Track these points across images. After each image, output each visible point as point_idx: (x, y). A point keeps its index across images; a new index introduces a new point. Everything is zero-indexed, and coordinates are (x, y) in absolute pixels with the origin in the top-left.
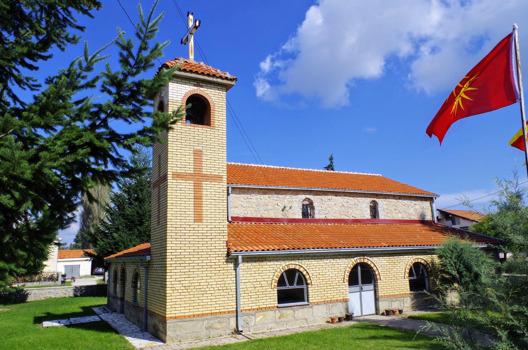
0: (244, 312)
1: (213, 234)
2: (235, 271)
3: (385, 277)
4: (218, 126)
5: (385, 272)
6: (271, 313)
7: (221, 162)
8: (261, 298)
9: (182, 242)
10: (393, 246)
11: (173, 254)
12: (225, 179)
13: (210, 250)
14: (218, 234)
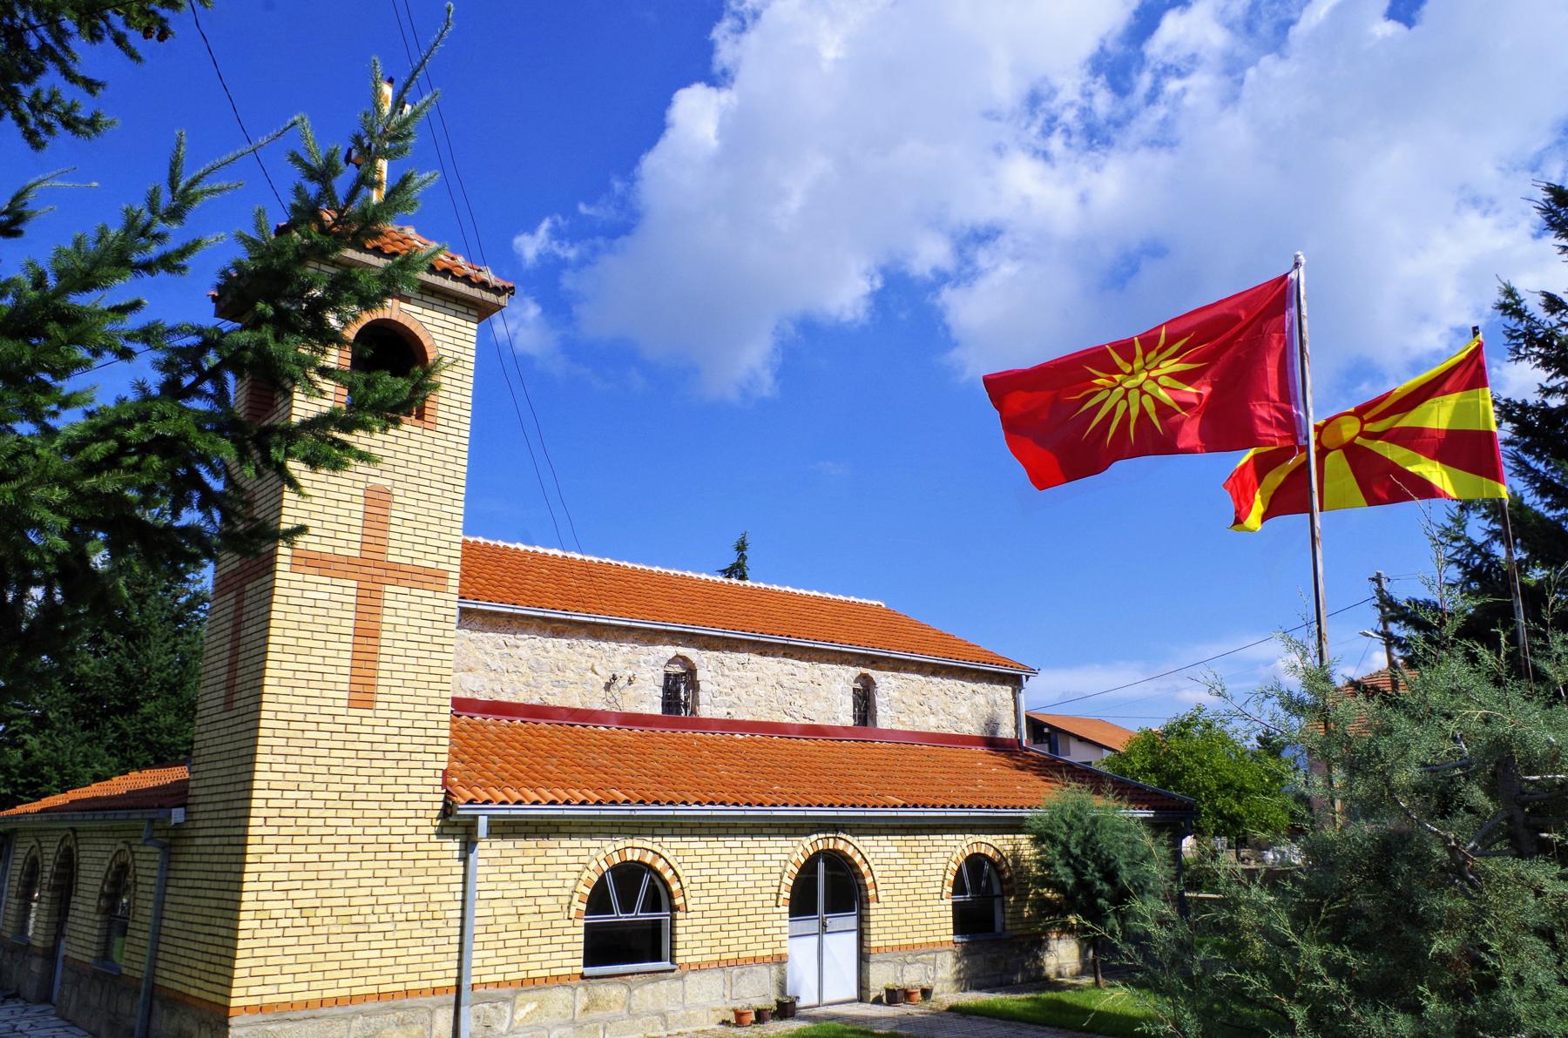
0: (480, 990)
1: (403, 748)
2: (461, 863)
3: (890, 893)
4: (445, 422)
5: (892, 880)
6: (561, 995)
7: (447, 530)
8: (536, 949)
9: (305, 769)
10: (915, 806)
11: (271, 803)
12: (454, 582)
13: (390, 797)
14: (421, 748)
